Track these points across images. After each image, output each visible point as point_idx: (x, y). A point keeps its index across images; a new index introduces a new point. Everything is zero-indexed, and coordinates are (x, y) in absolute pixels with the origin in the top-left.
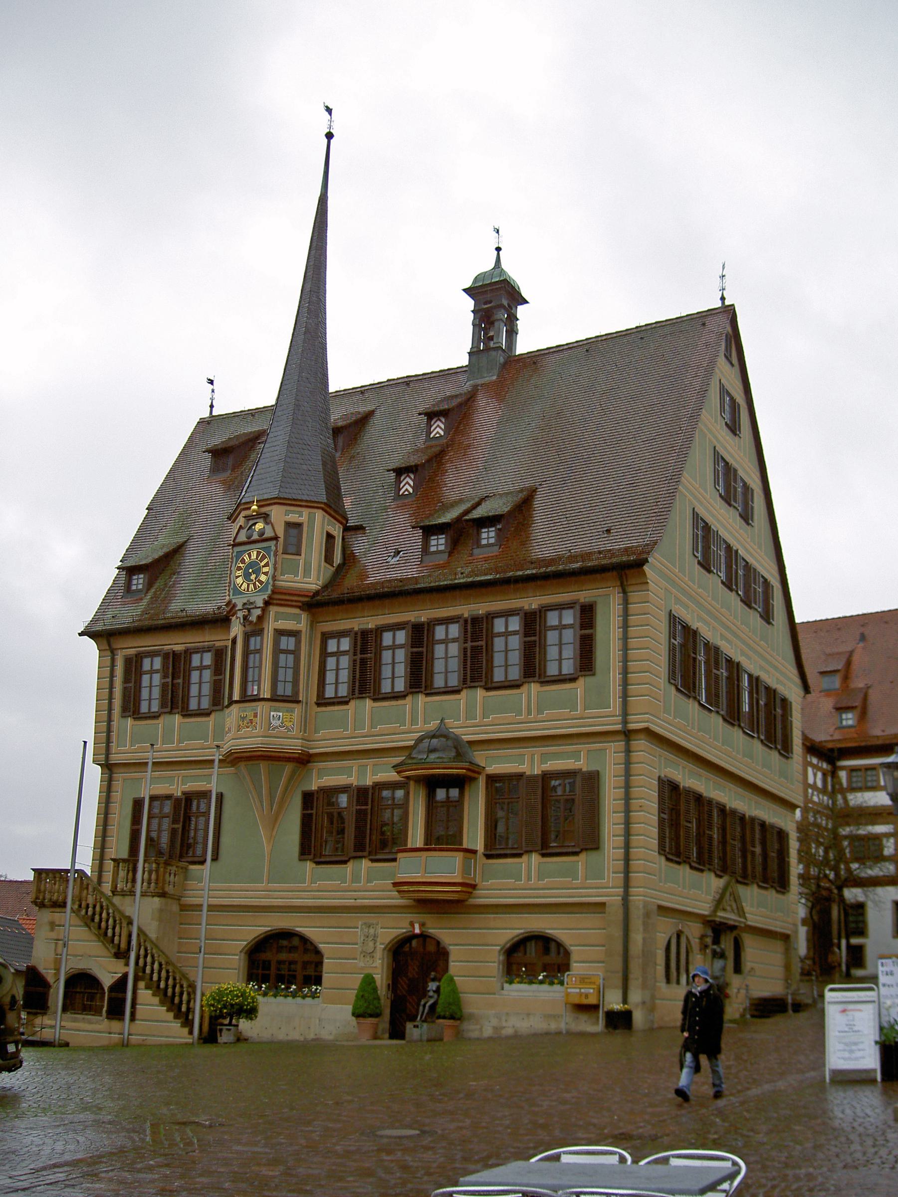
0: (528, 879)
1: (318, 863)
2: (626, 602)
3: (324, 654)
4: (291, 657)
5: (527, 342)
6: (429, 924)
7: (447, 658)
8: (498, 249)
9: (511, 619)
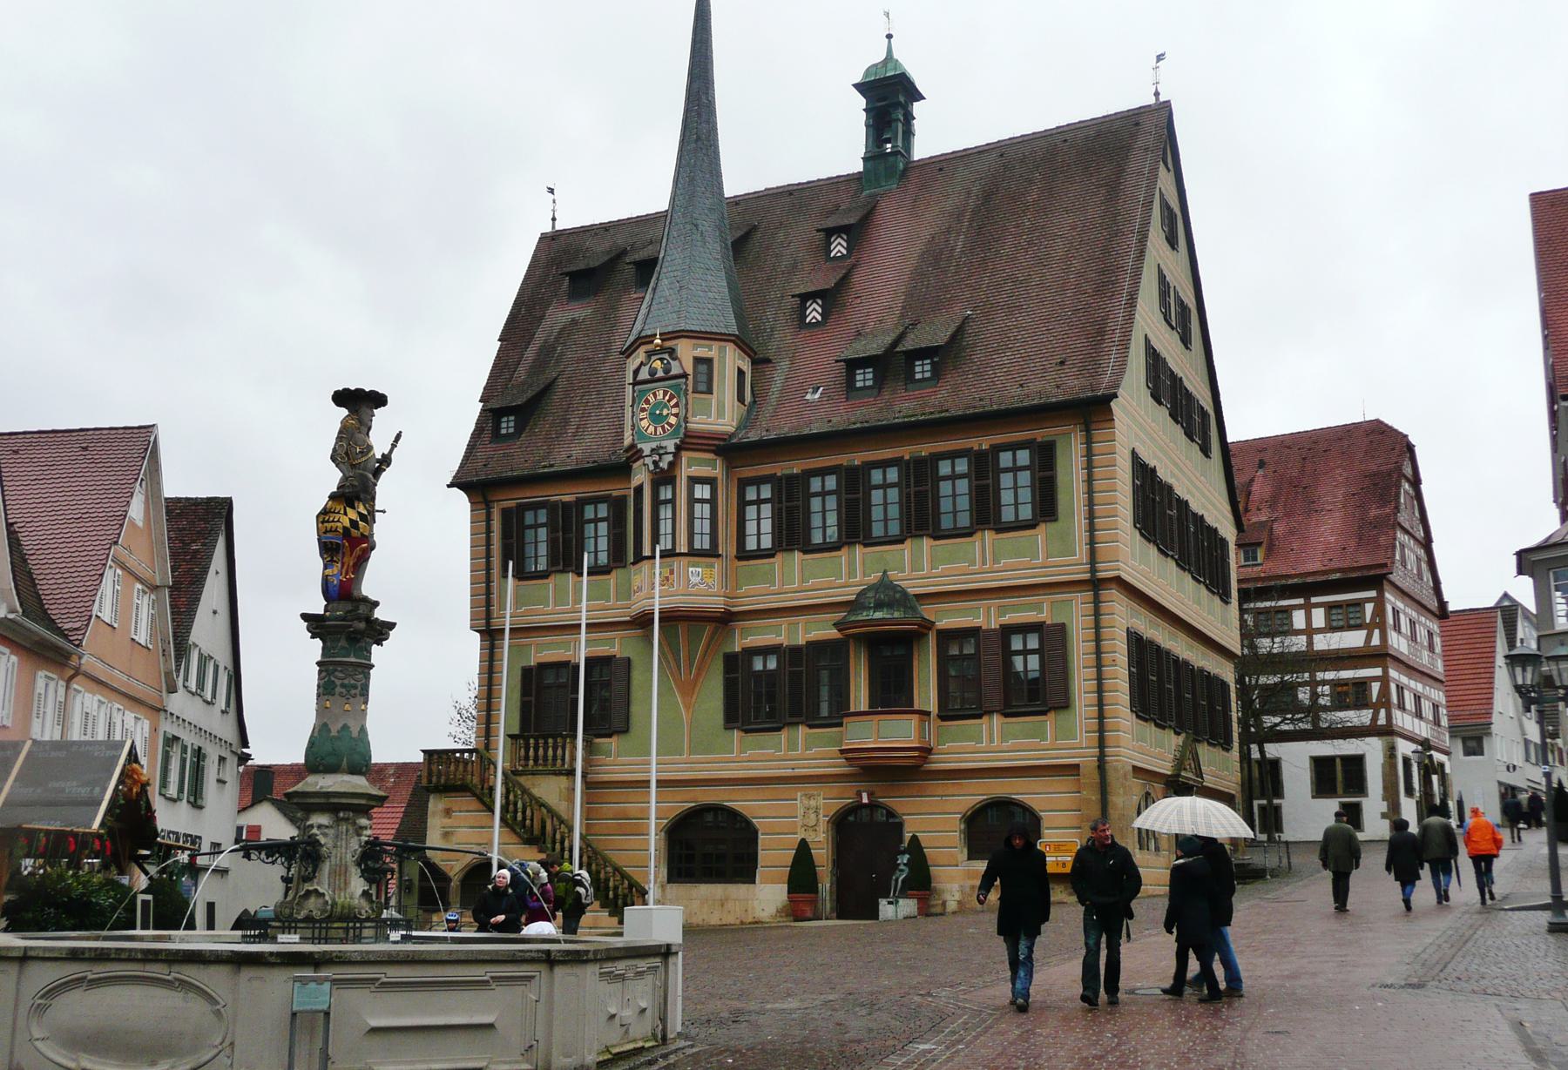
0: (991, 741)
1: (746, 731)
2: (1089, 442)
3: (743, 504)
4: (707, 507)
5: (925, 145)
6: (878, 794)
7: (885, 505)
8: (889, 37)
9: (957, 461)
